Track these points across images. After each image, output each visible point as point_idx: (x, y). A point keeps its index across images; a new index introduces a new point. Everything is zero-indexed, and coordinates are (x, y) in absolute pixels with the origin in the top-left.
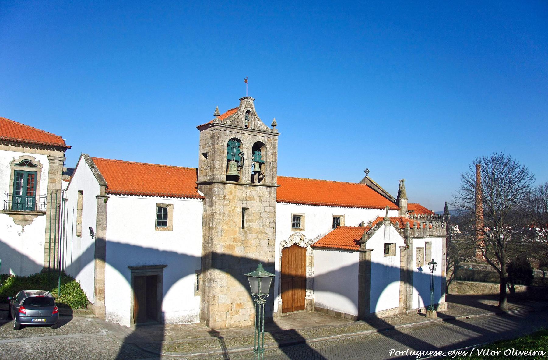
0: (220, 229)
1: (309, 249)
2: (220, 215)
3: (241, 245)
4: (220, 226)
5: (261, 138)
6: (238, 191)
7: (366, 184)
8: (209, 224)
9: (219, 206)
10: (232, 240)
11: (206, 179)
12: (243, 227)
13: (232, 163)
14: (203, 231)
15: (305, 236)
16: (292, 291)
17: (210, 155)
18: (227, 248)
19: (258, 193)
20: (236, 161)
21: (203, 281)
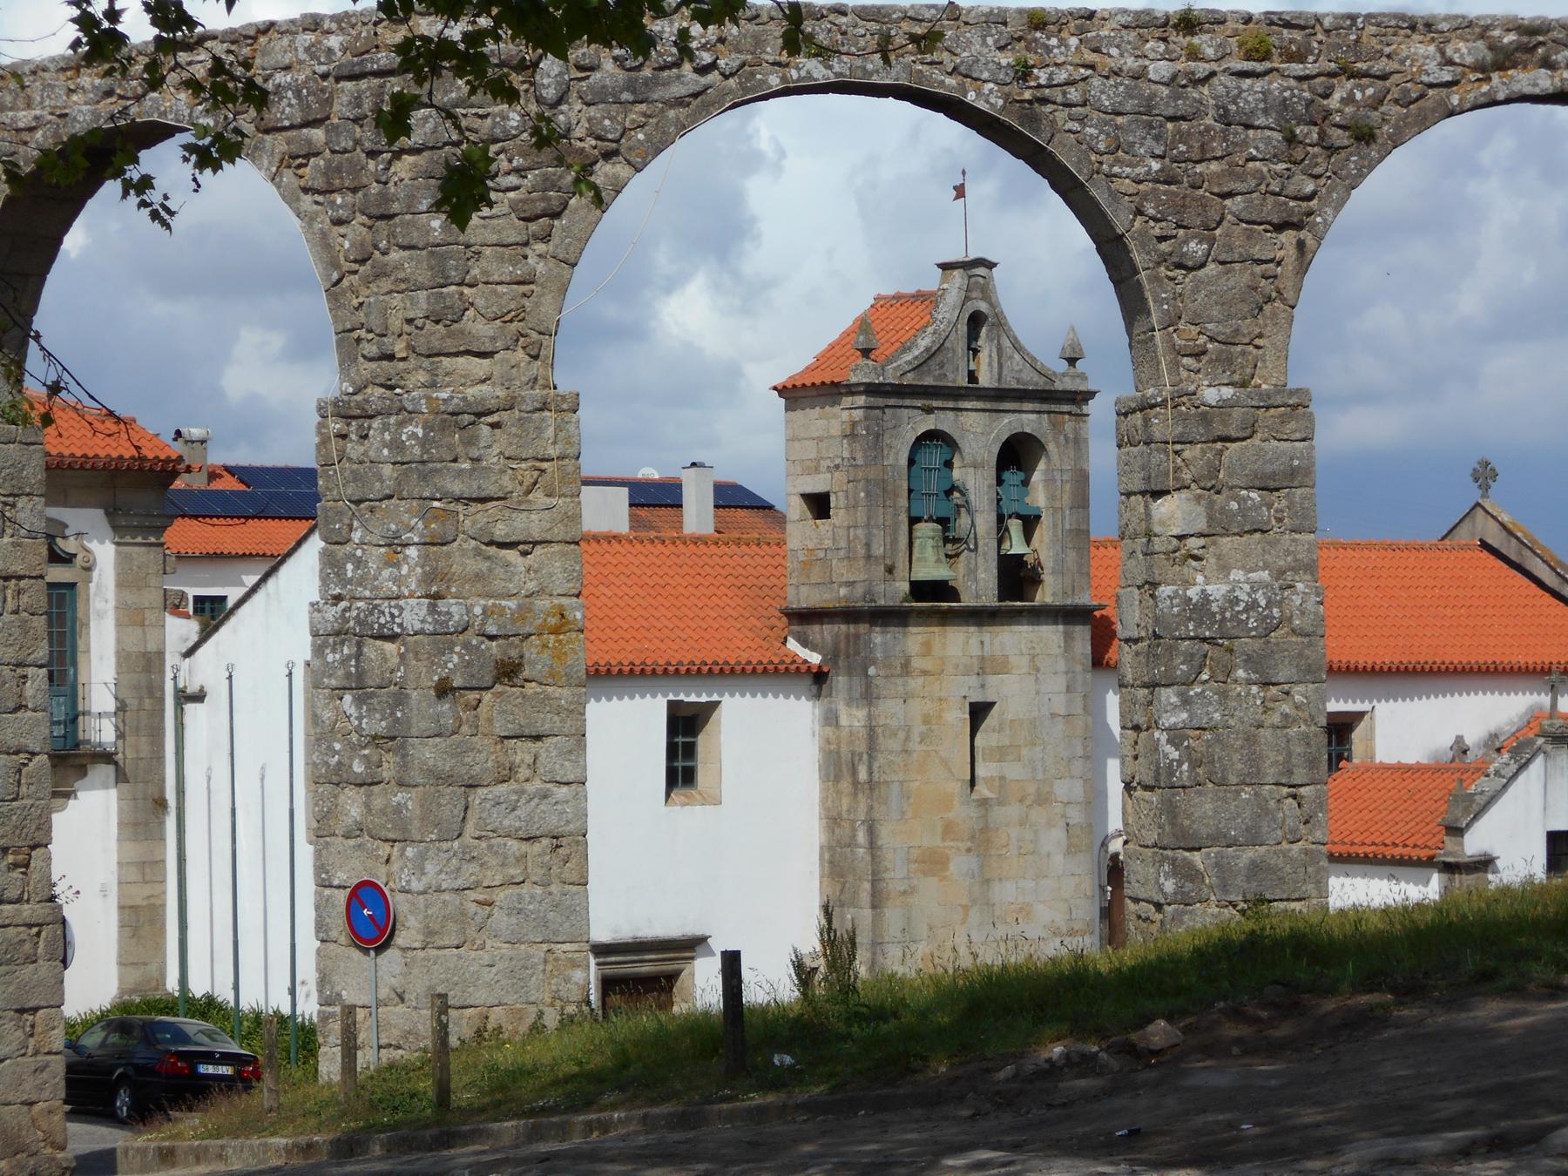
0: (895, 788)
3: (969, 850)
5: (1028, 421)
6: (959, 642)
7: (1481, 540)
8: (854, 772)
9: (890, 702)
10: (939, 830)
11: (827, 596)
14: (824, 801)
18: (924, 862)
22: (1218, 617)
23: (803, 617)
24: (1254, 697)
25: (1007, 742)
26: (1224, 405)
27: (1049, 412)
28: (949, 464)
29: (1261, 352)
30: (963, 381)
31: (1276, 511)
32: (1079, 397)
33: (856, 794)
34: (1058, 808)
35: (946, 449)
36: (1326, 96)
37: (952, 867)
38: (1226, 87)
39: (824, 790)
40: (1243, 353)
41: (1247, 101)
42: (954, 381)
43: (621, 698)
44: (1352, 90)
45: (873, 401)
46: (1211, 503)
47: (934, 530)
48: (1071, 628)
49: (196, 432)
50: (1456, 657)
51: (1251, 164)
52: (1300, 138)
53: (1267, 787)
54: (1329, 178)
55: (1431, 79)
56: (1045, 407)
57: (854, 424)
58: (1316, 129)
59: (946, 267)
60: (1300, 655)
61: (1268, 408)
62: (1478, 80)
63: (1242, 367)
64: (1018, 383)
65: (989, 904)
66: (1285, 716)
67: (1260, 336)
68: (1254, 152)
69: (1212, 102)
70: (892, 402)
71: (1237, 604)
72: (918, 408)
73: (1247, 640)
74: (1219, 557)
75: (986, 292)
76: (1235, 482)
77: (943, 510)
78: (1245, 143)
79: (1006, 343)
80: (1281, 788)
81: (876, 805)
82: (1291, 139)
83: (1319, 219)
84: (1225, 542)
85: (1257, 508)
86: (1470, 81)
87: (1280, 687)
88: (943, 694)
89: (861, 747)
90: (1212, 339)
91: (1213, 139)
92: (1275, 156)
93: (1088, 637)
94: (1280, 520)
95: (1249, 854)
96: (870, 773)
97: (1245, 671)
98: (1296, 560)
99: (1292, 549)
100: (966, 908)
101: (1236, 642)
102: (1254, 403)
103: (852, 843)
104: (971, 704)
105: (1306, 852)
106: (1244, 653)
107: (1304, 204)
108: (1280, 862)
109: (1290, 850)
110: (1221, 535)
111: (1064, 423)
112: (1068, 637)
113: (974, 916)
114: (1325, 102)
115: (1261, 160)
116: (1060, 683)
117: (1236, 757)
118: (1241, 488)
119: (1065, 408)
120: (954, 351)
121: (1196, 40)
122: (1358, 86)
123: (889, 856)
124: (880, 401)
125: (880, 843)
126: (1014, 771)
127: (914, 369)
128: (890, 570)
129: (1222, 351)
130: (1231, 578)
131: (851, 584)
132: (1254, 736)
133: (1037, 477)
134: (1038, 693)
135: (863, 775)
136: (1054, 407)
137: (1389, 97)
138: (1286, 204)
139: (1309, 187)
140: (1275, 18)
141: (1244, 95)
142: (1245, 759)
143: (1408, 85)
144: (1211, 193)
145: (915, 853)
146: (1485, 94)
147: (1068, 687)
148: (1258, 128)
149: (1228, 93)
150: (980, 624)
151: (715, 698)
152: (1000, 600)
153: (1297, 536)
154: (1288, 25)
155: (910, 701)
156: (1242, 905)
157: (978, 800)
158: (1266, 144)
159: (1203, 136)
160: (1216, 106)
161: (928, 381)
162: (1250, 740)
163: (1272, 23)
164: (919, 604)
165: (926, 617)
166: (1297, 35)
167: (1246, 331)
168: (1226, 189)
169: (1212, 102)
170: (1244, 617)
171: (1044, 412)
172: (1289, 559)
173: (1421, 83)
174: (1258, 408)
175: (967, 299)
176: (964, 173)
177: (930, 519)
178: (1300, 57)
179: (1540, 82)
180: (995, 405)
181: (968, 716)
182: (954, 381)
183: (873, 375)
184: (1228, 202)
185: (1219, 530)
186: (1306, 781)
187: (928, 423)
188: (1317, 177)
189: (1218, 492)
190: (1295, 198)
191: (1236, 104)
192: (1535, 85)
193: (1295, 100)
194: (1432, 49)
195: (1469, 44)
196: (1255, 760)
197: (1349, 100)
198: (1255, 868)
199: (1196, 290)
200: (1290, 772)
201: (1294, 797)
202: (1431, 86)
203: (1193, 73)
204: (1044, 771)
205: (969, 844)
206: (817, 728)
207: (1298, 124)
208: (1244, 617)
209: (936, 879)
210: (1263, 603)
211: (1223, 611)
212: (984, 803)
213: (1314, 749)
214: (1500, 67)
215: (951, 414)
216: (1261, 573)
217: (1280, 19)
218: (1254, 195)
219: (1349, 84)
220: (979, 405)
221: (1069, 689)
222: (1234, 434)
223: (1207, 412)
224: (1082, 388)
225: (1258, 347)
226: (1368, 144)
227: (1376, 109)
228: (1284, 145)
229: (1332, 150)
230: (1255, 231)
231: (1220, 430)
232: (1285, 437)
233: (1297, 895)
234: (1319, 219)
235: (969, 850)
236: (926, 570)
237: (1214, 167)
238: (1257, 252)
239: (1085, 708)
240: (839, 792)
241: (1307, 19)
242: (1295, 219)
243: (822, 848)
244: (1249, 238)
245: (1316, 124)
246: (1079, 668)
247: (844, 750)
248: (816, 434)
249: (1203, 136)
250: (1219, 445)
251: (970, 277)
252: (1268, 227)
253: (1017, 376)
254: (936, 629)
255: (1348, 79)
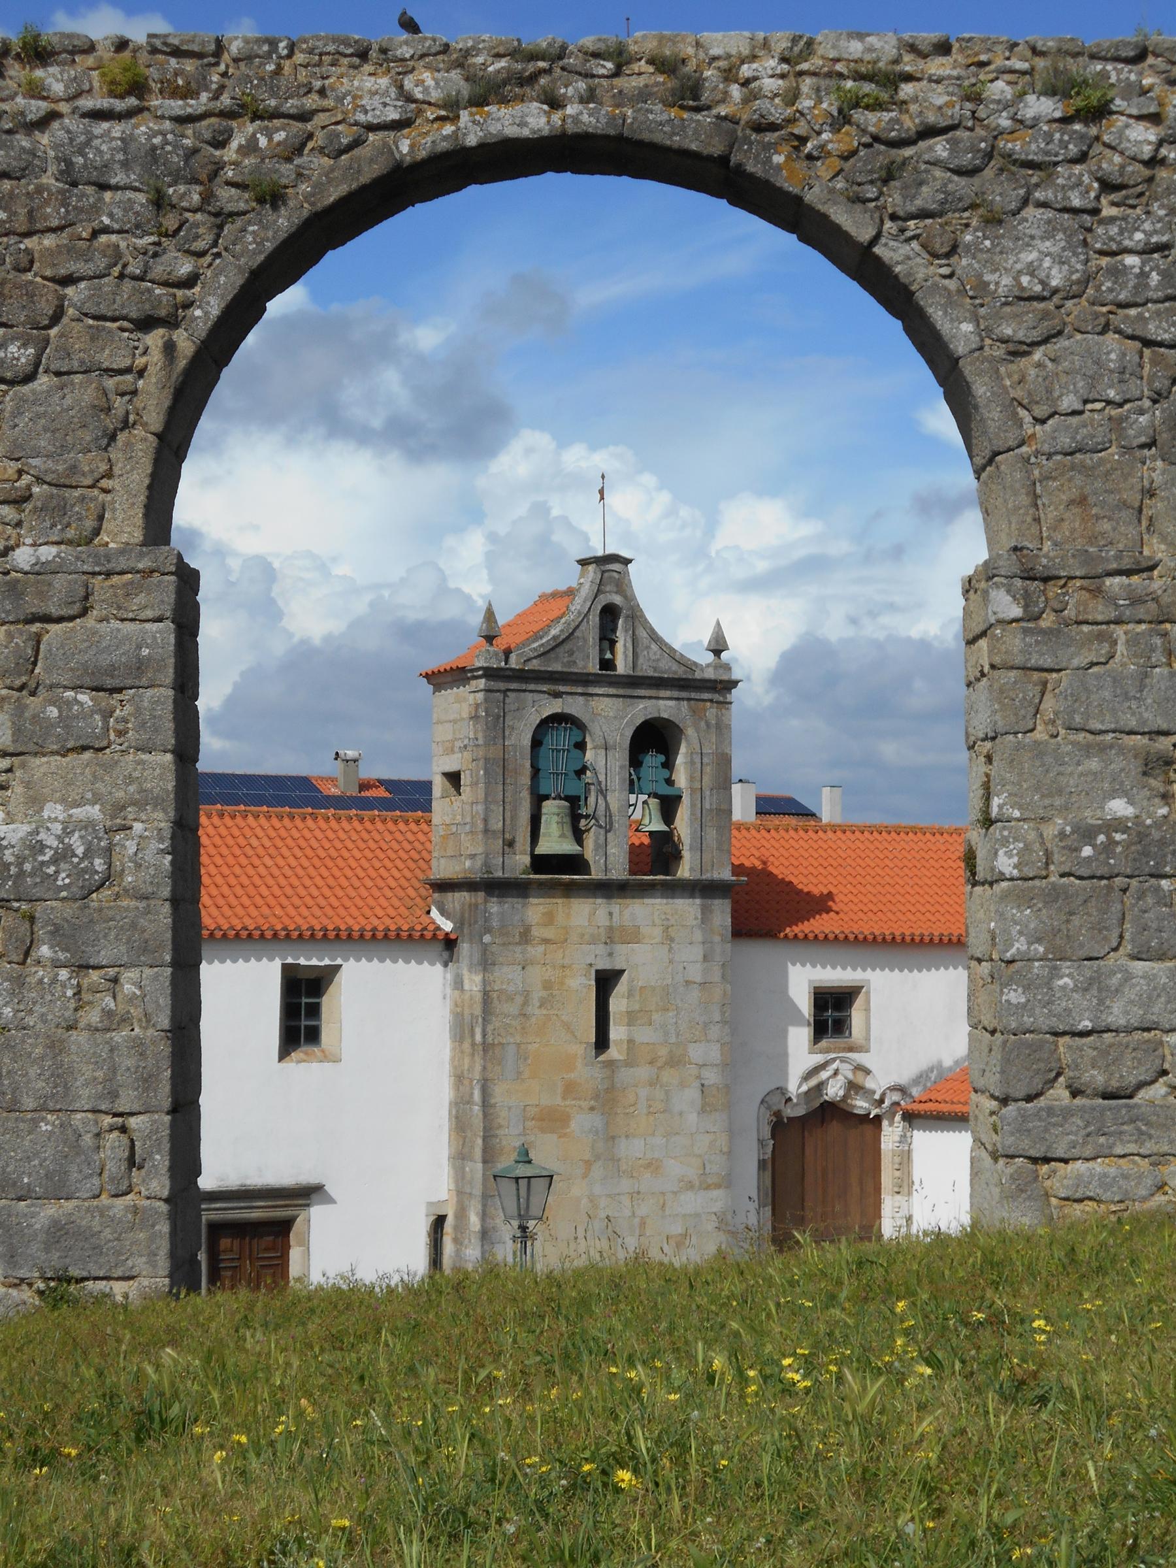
0: (511, 1050)
1: (891, 1134)
2: (511, 999)
3: (592, 1109)
4: (512, 1040)
5: (665, 707)
8: (473, 1035)
9: (505, 969)
11: (457, 868)
12: (602, 1042)
13: (550, 808)
14: (452, 1059)
15: (867, 1072)
16: (167, 1027)
17: (468, 783)
19: (657, 913)
20: (567, 798)
21: (456, 1241)
22: (13, 870)
23: (443, 886)
24: (64, 986)
25: (637, 1007)
26: (41, 571)
27: (689, 699)
28: (581, 746)
29: (109, 497)
30: (593, 667)
31: (117, 721)
32: (719, 686)
33: (473, 1055)
34: (693, 1070)
35: (576, 731)
36: (221, 144)
37: (574, 1125)
38: (68, 132)
39: (453, 1049)
40: (82, 499)
41: (99, 152)
42: (585, 667)
43: (259, 959)
44: (254, 135)
45: (493, 685)
46: (20, 709)
47: (559, 807)
48: (709, 901)
49: (351, 754)
50: (921, 928)
51: (103, 238)
52: (175, 200)
53: (79, 1116)
54: (218, 255)
55: (370, 118)
56: (684, 694)
57: (477, 706)
58: (198, 188)
59: (583, 563)
60: (134, 925)
61: (108, 574)
62: (439, 119)
63: (80, 519)
64: (655, 670)
65: (615, 1160)
66: (108, 1014)
67: (109, 475)
68: (106, 220)
69: (52, 153)
70: (514, 686)
71: (42, 852)
72: (544, 692)
73: (54, 904)
74: (28, 785)
75: (622, 585)
76: (55, 679)
77: (573, 788)
78: (96, 209)
79: (642, 633)
80: (103, 1116)
81: (489, 1066)
82: (159, 202)
83: (198, 313)
84: (40, 765)
85: (87, 715)
86: (428, 120)
87: (103, 972)
88: (567, 962)
89: (478, 1010)
90: (39, 480)
91: (47, 202)
92: (137, 226)
93: (729, 910)
94: (121, 733)
95: (50, 1211)
96: (484, 1035)
97: (51, 947)
98: (141, 791)
99: (136, 774)
100: (588, 1164)
101: (39, 907)
102: (86, 568)
103: (470, 1102)
104: (597, 971)
105: (135, 1210)
106: (48, 922)
107: (180, 293)
108: (96, 1224)
109: (110, 1208)
110: (36, 754)
111: (705, 711)
112: (705, 910)
113: (597, 1171)
114: (217, 153)
115: (119, 232)
116: (697, 952)
117: (33, 1071)
118: (65, 687)
119: (706, 696)
120: (585, 640)
121: (39, 73)
122: (262, 130)
123: (504, 1114)
124: (502, 685)
125: (493, 1101)
126: (644, 1035)
127: (539, 656)
128: (510, 844)
129: (52, 496)
130: (46, 814)
131: (473, 857)
132: (62, 1041)
133: (680, 760)
134: (671, 962)
135: (478, 1038)
136: (693, 695)
137: (310, 145)
138: (149, 290)
139: (185, 268)
140: (158, 43)
141: (96, 142)
142: (47, 1074)
143: (340, 127)
144: (44, 278)
145: (532, 1111)
146: (445, 138)
147: (705, 956)
148: (116, 188)
149: (71, 140)
150: (609, 896)
151: (339, 961)
152: (632, 872)
153: (146, 757)
154: (177, 52)
155: (529, 968)
156: (41, 1285)
157: (604, 1062)
158: (125, 210)
159: (32, 199)
160: (56, 158)
161: (557, 667)
162: (56, 1047)
163: (154, 51)
164: (537, 876)
165: (548, 889)
166: (189, 66)
167: (86, 469)
168: (63, 272)
169: (52, 153)
170: (51, 870)
171: (683, 699)
172: (132, 789)
173: (356, 124)
174: (94, 574)
175: (599, 592)
176: (603, 477)
177: (558, 797)
178: (187, 93)
179: (530, 120)
180: (629, 692)
181: (593, 983)
182: (585, 667)
183: (493, 660)
184: (70, 291)
185: (32, 747)
186: (136, 1107)
187: (555, 707)
188: (201, 254)
189: (33, 694)
190: (166, 284)
191: (84, 155)
192: (523, 124)
193: (169, 148)
194: (384, 82)
195: (438, 75)
196: (61, 1078)
197: (250, 147)
198: (58, 1232)
199: (17, 412)
200: (114, 1095)
201: (123, 1129)
202: (371, 128)
203: (22, 114)
204: (678, 1035)
205: (592, 1103)
206: (449, 991)
207: (174, 183)
208: (51, 870)
209: (555, 1137)
210: (80, 851)
211: (20, 860)
212: (611, 1064)
213: (151, 1061)
214: (478, 102)
215: (581, 699)
216: (88, 808)
217: (165, 44)
218: (106, 280)
219: (250, 128)
220: (612, 691)
221: (706, 958)
222: (54, 611)
223: (17, 581)
224: (725, 677)
225: (106, 491)
226: (275, 207)
227: (289, 160)
228: (148, 213)
229: (222, 218)
230: (104, 328)
231: (33, 605)
232: (131, 615)
233: (118, 1273)
234: (198, 313)
235: (592, 1109)
236: (549, 844)
237: (49, 241)
238: (106, 358)
239: (723, 977)
240: (462, 1052)
241: (203, 43)
242: (163, 313)
243: (450, 1104)
244: (93, 339)
245: (197, 181)
246: (717, 939)
247: (467, 1012)
248: (452, 718)
249: (32, 199)
250: (35, 627)
251: (603, 572)
252: (125, 324)
253: (654, 664)
254: (559, 901)
255: (252, 121)
